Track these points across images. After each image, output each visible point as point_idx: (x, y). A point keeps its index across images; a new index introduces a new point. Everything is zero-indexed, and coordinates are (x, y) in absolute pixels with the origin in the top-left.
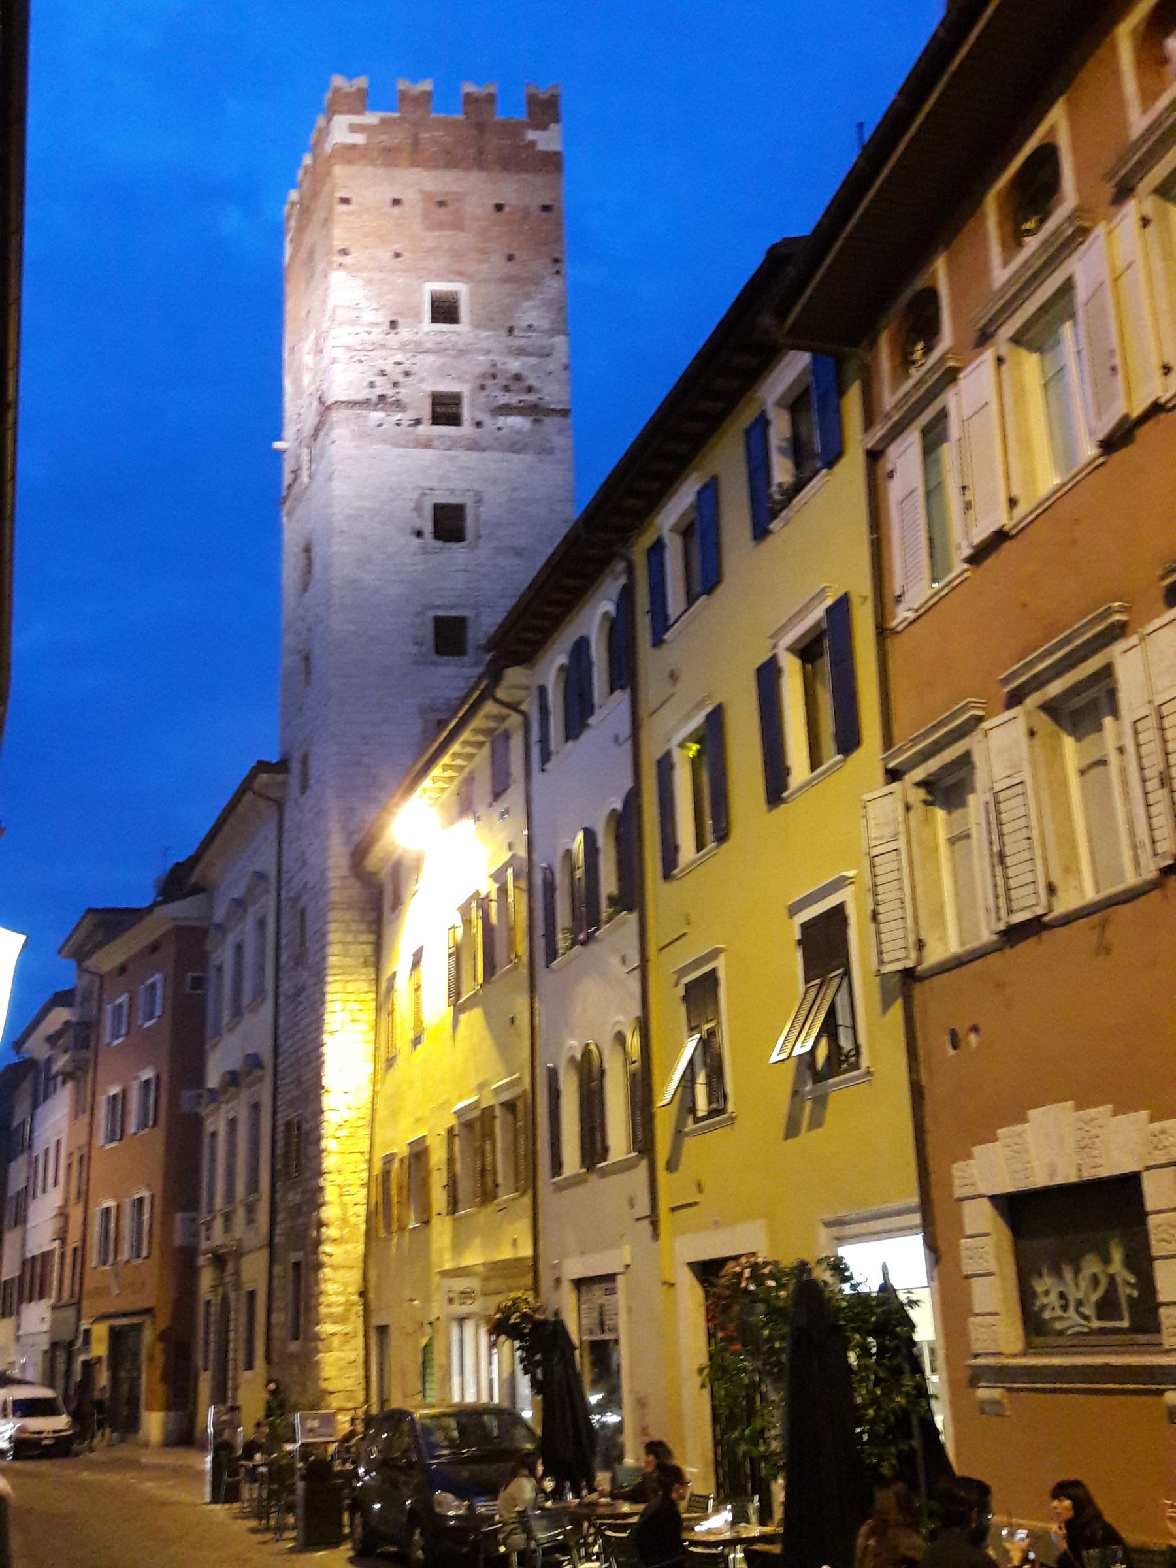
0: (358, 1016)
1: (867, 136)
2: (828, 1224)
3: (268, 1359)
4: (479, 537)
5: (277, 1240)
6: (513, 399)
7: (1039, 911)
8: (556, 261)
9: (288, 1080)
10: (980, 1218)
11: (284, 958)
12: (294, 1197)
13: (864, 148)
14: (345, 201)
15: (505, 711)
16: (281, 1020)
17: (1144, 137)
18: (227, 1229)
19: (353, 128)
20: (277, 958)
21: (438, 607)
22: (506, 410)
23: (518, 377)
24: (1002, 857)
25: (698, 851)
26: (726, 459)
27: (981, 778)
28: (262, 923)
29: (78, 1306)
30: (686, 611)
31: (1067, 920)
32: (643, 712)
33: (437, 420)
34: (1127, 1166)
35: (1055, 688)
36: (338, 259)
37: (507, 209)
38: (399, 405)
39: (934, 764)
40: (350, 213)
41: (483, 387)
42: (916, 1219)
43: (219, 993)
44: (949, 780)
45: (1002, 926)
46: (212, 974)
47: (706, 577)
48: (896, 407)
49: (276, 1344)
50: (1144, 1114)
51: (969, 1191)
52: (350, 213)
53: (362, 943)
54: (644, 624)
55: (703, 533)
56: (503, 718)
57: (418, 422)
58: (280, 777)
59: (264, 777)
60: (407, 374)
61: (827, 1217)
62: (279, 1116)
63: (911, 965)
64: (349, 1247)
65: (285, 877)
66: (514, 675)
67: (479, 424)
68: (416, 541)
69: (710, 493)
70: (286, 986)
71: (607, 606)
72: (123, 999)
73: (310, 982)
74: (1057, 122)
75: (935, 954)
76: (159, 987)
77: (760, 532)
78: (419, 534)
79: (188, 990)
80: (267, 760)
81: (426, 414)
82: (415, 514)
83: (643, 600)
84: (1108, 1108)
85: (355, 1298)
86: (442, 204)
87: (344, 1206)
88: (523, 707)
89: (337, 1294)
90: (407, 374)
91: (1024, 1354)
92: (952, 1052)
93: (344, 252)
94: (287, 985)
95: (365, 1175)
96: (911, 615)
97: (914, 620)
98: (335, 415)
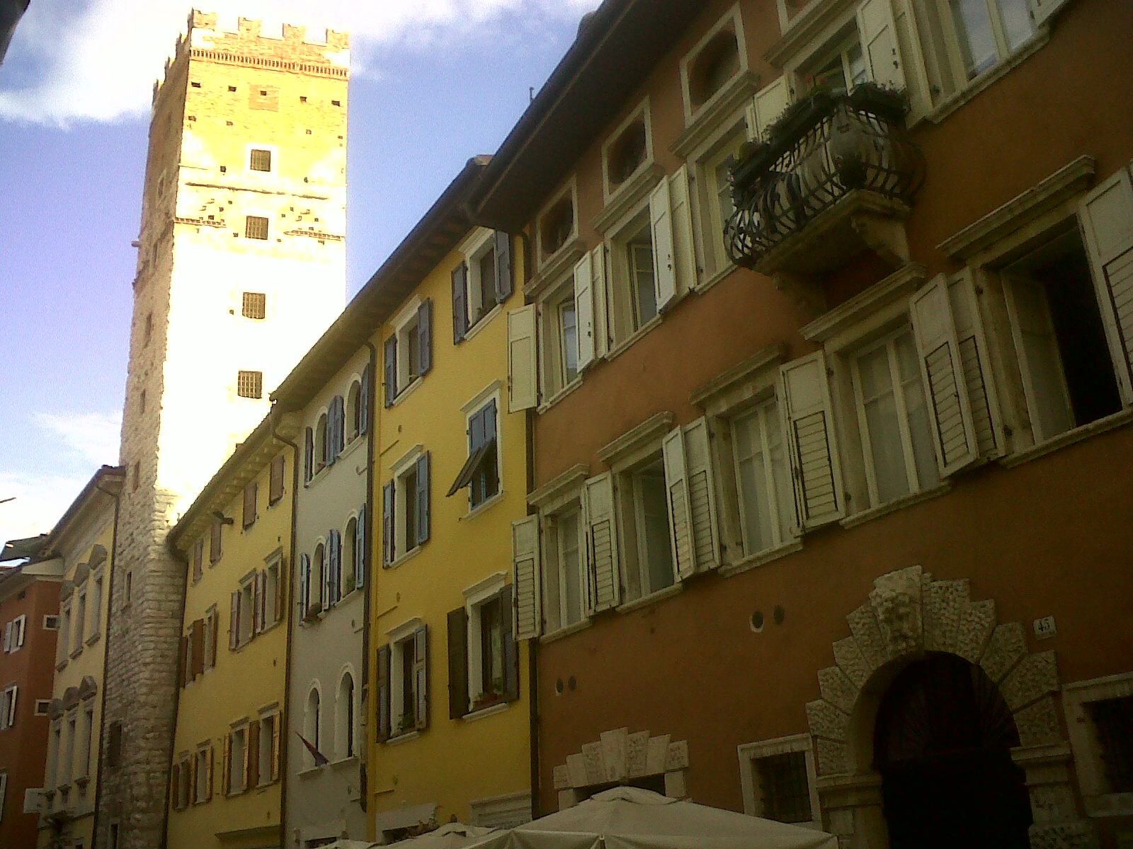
1: (534, 97)
2: (474, 806)
6: (305, 224)
7: (614, 604)
11: (114, 609)
12: (114, 780)
13: (533, 102)
15: (282, 443)
18: (65, 800)
20: (110, 609)
24: (594, 567)
25: (407, 551)
26: (441, 293)
27: (584, 515)
28: (100, 582)
30: (409, 385)
31: (631, 611)
33: (265, 221)
35: (631, 461)
39: (558, 504)
40: (199, 94)
44: (567, 515)
45: (592, 613)
46: (62, 614)
47: (422, 365)
48: (545, 271)
50: (667, 737)
51: (562, 785)
53: (171, 601)
54: (380, 392)
55: (420, 338)
56: (281, 448)
58: (118, 479)
62: (106, 721)
63: (536, 636)
65: (119, 550)
69: (428, 307)
70: (115, 628)
74: (644, 110)
75: (551, 632)
77: (459, 341)
79: (45, 627)
80: (110, 465)
81: (241, 228)
83: (380, 377)
84: (646, 733)
86: (264, 93)
87: (150, 786)
88: (294, 441)
92: (558, 694)
94: (115, 628)
96: (549, 406)
97: (550, 409)
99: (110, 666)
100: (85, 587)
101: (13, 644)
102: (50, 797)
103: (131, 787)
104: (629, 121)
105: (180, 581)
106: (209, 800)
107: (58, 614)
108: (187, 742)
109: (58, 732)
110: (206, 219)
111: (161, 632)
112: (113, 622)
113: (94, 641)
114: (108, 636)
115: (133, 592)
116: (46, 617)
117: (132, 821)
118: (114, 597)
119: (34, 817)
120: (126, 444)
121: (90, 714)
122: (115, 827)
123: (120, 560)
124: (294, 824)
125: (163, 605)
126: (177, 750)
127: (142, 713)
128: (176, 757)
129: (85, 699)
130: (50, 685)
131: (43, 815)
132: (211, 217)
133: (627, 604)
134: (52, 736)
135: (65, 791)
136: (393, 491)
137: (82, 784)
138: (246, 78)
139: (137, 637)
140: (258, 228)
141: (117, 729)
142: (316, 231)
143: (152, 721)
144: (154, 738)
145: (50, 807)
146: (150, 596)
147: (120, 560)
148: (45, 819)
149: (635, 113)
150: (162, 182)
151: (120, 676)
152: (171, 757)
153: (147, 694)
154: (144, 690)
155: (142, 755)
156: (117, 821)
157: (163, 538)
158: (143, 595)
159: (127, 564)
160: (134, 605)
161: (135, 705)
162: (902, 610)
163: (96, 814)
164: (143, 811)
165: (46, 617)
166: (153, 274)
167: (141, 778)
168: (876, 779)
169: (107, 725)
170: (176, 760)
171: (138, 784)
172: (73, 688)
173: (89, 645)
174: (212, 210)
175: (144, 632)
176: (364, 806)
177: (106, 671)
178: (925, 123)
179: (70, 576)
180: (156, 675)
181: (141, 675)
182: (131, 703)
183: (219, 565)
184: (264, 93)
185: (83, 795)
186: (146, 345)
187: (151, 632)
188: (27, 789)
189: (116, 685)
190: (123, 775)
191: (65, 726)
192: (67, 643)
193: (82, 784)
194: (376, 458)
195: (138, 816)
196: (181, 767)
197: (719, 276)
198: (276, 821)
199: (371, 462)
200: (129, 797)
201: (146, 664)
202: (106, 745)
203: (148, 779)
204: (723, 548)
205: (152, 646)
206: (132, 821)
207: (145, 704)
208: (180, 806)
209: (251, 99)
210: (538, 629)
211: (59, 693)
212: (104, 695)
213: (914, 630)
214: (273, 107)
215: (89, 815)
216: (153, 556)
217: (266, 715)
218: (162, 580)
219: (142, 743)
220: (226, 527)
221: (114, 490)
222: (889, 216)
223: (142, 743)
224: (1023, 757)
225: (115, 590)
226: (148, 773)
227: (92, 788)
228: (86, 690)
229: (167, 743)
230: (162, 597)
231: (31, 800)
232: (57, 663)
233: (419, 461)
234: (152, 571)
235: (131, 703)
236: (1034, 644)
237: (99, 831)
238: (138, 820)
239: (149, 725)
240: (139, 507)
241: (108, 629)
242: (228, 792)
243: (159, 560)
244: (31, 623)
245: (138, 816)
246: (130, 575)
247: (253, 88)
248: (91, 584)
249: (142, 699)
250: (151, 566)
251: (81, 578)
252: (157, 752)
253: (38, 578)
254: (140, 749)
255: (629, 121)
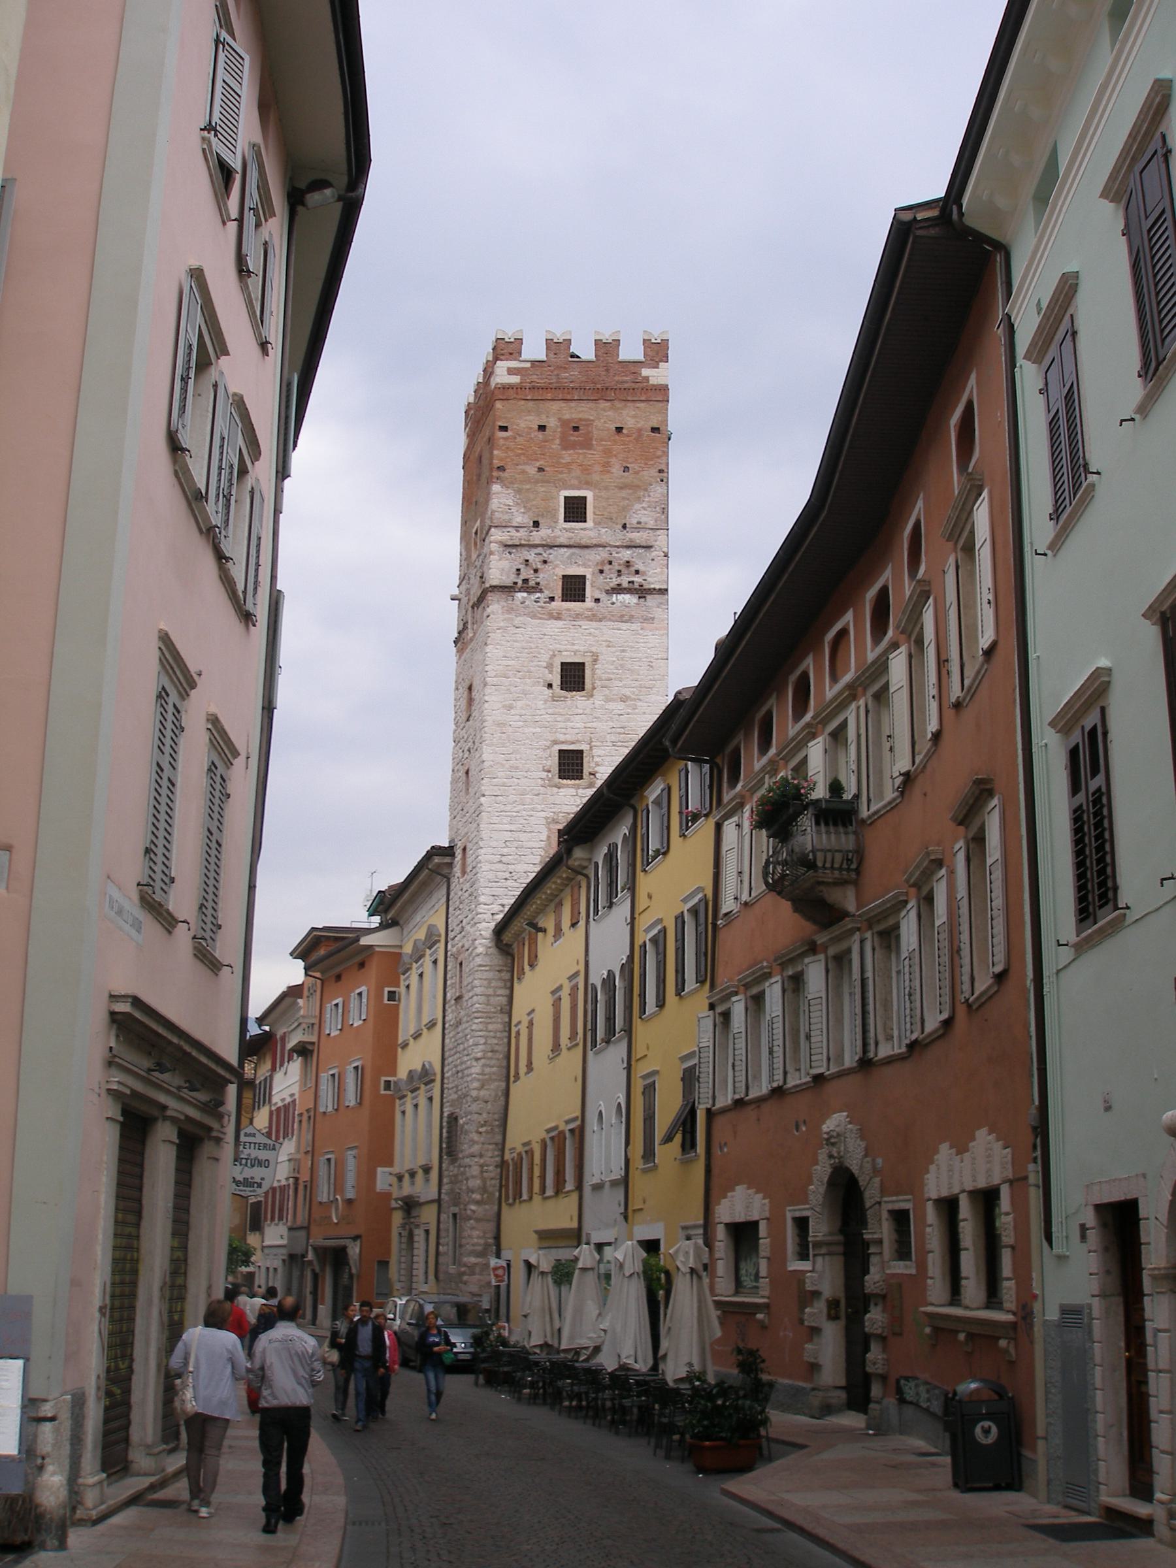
0: (497, 1048)
3: (437, 1277)
4: (594, 688)
5: (443, 1196)
8: (661, 471)
9: (450, 1086)
10: (721, 1233)
14: (504, 429)
16: (447, 1041)
17: (832, 702)
19: (510, 371)
21: (563, 743)
22: (618, 590)
23: (628, 564)
29: (307, 1228)
32: (638, 910)
34: (756, 1218)
36: (495, 474)
37: (624, 431)
38: (537, 588)
41: (601, 571)
42: (701, 1231)
43: (407, 1006)
49: (442, 1268)
52: (506, 439)
57: (552, 599)
58: (447, 860)
59: (437, 860)
60: (545, 562)
61: (683, 1224)
64: (487, 1207)
65: (451, 935)
66: (579, 853)
67: (597, 600)
68: (548, 692)
71: (624, 830)
72: (339, 1000)
73: (465, 1019)
76: (364, 995)
78: (550, 686)
79: (386, 1002)
81: (558, 593)
82: (547, 671)
85: (491, 1241)
86: (576, 429)
87: (484, 1180)
89: (479, 1237)
90: (545, 562)
91: (734, 1295)
93: (501, 469)
95: (498, 1159)
98: (490, 597)
99: (447, 1054)
100: (422, 965)
101: (357, 1018)
102: (400, 1178)
103: (467, 1179)
104: (798, 672)
105: (507, 976)
106: (531, 1198)
107: (398, 986)
108: (516, 1139)
109: (403, 1112)
110: (520, 582)
111: (490, 1027)
112: (449, 1011)
113: (431, 1025)
114: (444, 1024)
115: (465, 983)
116: (387, 989)
117: (469, 1212)
118: (449, 983)
119: (387, 1196)
120: (455, 822)
121: (431, 1099)
122: (455, 1215)
123: (453, 946)
124: (586, 1228)
125: (493, 1000)
126: (508, 1145)
127: (475, 1107)
128: (507, 1152)
129: (426, 1084)
130: (392, 1069)
131: (394, 1196)
132: (526, 581)
133: (751, 1096)
134: (398, 1115)
135: (413, 1174)
136: (684, 922)
137: (427, 1170)
138: (555, 414)
139: (468, 1031)
140: (574, 588)
141: (453, 1119)
142: (636, 586)
143: (485, 1115)
144: (487, 1132)
145: (401, 1187)
146: (478, 990)
147: (453, 946)
148: (396, 1200)
149: (735, 742)
150: (476, 533)
151: (456, 1066)
152: (503, 1150)
153: (479, 1089)
154: (476, 1084)
155: (475, 1149)
156: (456, 1210)
157: (490, 931)
158: (473, 988)
159: (459, 953)
160: (466, 997)
161: (469, 1099)
162: (833, 1140)
163: (439, 1201)
164: (478, 1203)
165: (387, 989)
166: (471, 640)
167: (475, 1170)
168: (840, 1238)
169: (445, 1114)
170: (507, 1156)
171: (473, 1177)
172: (415, 1071)
173: (428, 1029)
174: (526, 573)
175: (474, 1027)
176: (626, 1218)
177: (443, 1059)
178: (863, 821)
179: (408, 949)
180: (487, 1070)
181: (473, 1070)
182: (466, 1096)
183: (538, 969)
184: (576, 429)
185: (427, 1180)
186: (468, 720)
187: (481, 1027)
188: (379, 1170)
189: (453, 1075)
190: (460, 1166)
191: (409, 1108)
192: (407, 1024)
193: (427, 1170)
194: (636, 916)
195: (473, 1207)
196: (524, 1156)
197: (885, 806)
198: (575, 1225)
199: (633, 918)
200: (464, 1188)
201: (477, 1059)
202: (445, 1135)
203: (482, 1172)
204: (785, 1073)
205: (482, 1041)
206: (469, 1212)
207: (476, 1099)
208: (511, 1201)
209: (564, 438)
210: (711, 1101)
211: (402, 1074)
212: (442, 1083)
213: (839, 1153)
214: (587, 444)
215: (432, 1201)
216: (480, 950)
217: (572, 1126)
218: (490, 975)
219: (476, 1137)
220: (540, 935)
221: (445, 871)
222: (842, 883)
223: (476, 1137)
224: (870, 1236)
225: (449, 976)
226: (481, 1166)
227: (434, 1174)
228: (424, 1076)
229: (499, 1138)
230: (490, 991)
231: (383, 1179)
232: (400, 1041)
233: (700, 901)
234: (480, 966)
235: (466, 1096)
236: (876, 1171)
237: (442, 1219)
238: (474, 1212)
239: (481, 1119)
240: (466, 895)
241: (444, 1017)
242: (544, 1193)
243: (486, 954)
244: (372, 994)
245: (473, 1207)
246: (461, 964)
247: (564, 423)
248: (427, 961)
249: (474, 1093)
250: (478, 960)
251: (418, 957)
252: (491, 1147)
253: (377, 949)
254: (474, 1142)
255: (798, 672)
